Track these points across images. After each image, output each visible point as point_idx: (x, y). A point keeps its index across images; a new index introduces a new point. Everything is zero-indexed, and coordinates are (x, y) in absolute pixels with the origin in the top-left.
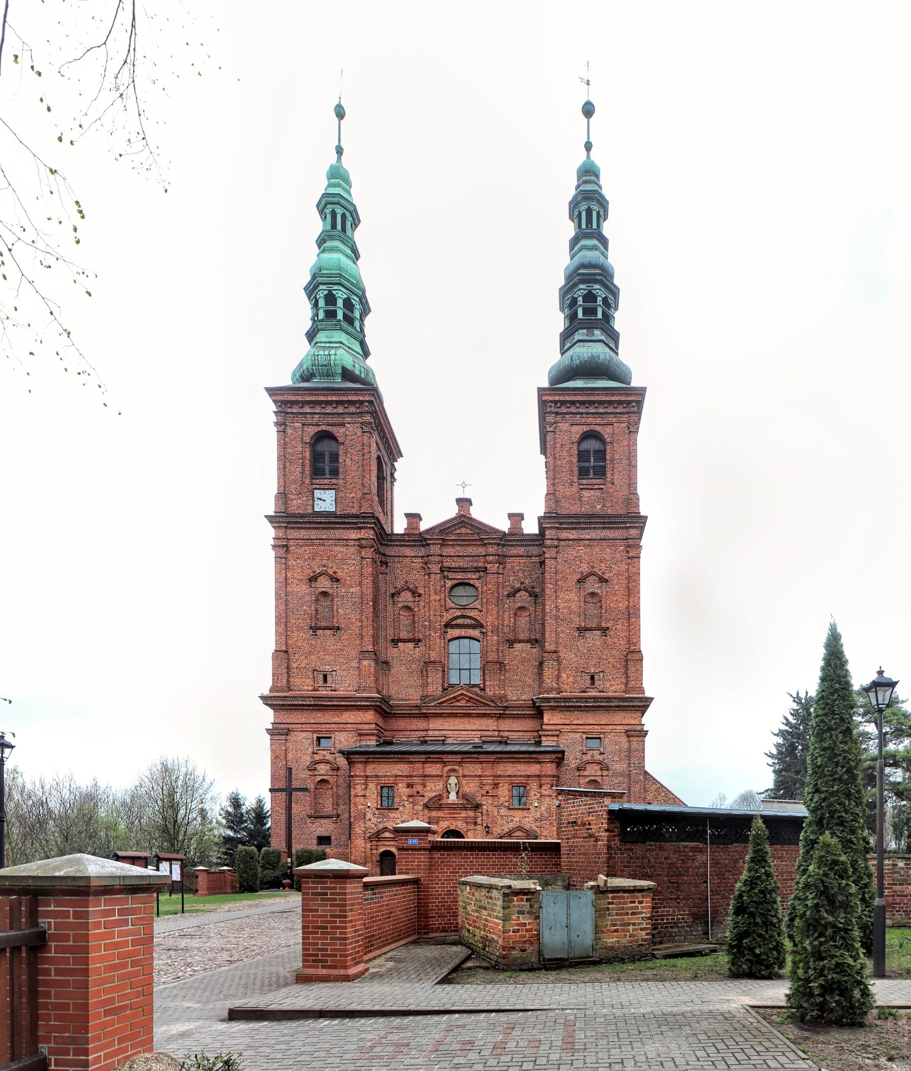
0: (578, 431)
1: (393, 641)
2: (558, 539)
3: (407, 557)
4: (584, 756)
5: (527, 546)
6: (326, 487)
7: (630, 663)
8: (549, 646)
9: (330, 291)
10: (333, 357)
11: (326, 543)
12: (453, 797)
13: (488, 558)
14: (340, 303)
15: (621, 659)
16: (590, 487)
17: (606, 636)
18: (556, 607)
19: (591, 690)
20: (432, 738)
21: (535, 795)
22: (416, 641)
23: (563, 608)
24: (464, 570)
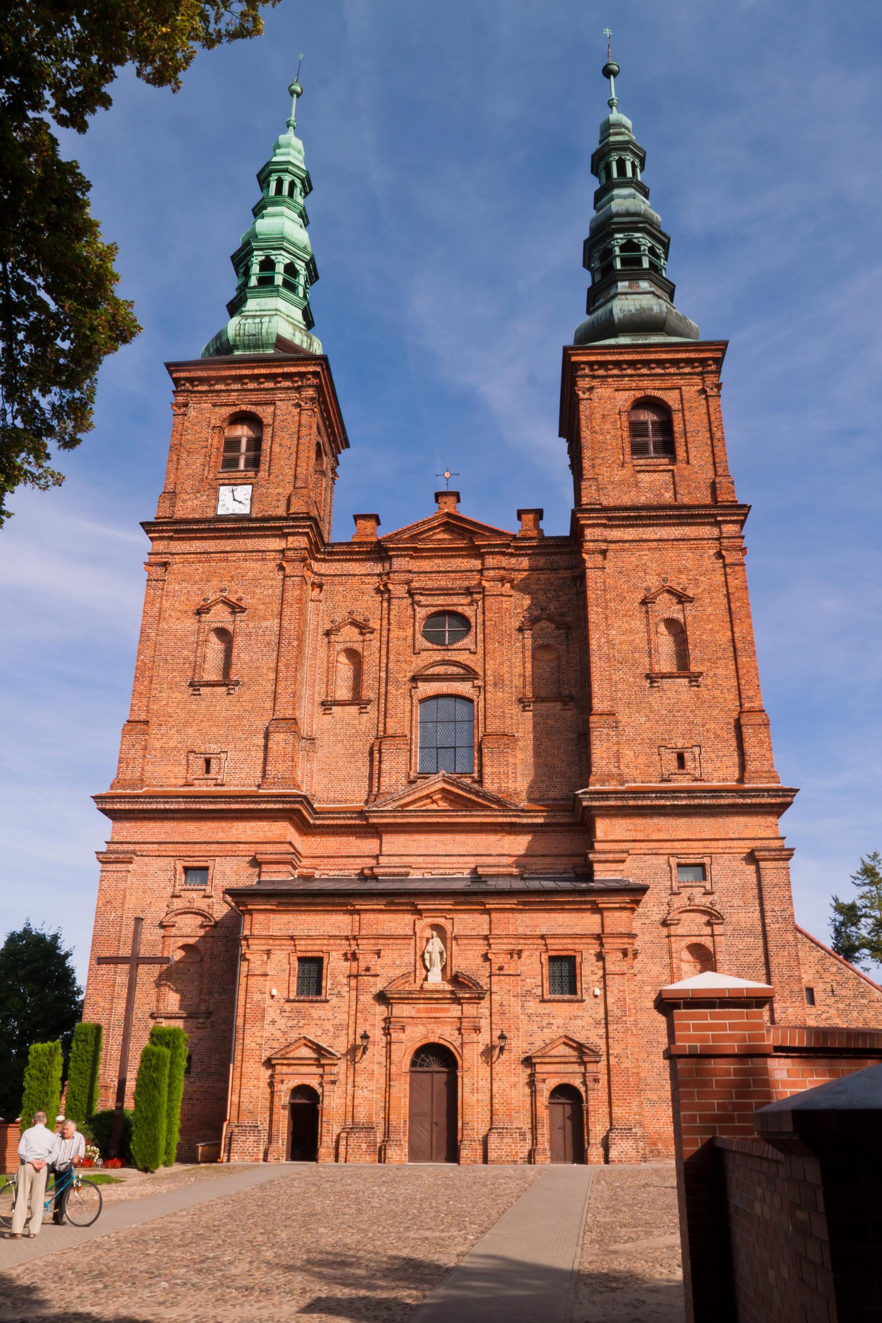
0: (625, 399)
1: (323, 704)
2: (605, 541)
3: (354, 575)
4: (675, 899)
5: (549, 554)
6: (239, 481)
7: (747, 731)
8: (598, 705)
9: (268, 257)
10: (265, 326)
11: (231, 557)
12: (435, 978)
13: (486, 573)
14: (280, 268)
15: (728, 724)
16: (653, 468)
17: (698, 686)
18: (609, 642)
19: (680, 777)
20: (386, 870)
21: (593, 973)
22: (358, 700)
23: (621, 644)
24: (447, 592)
